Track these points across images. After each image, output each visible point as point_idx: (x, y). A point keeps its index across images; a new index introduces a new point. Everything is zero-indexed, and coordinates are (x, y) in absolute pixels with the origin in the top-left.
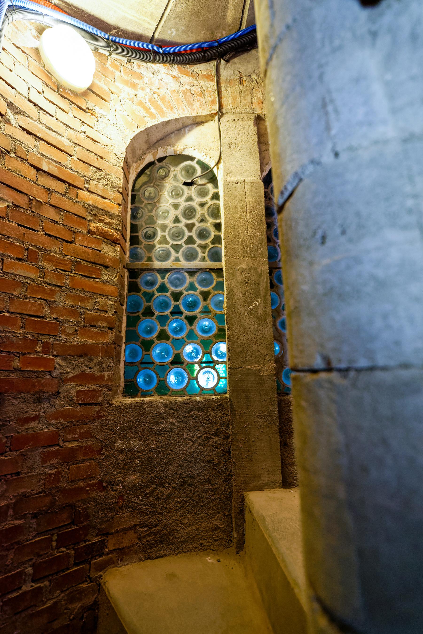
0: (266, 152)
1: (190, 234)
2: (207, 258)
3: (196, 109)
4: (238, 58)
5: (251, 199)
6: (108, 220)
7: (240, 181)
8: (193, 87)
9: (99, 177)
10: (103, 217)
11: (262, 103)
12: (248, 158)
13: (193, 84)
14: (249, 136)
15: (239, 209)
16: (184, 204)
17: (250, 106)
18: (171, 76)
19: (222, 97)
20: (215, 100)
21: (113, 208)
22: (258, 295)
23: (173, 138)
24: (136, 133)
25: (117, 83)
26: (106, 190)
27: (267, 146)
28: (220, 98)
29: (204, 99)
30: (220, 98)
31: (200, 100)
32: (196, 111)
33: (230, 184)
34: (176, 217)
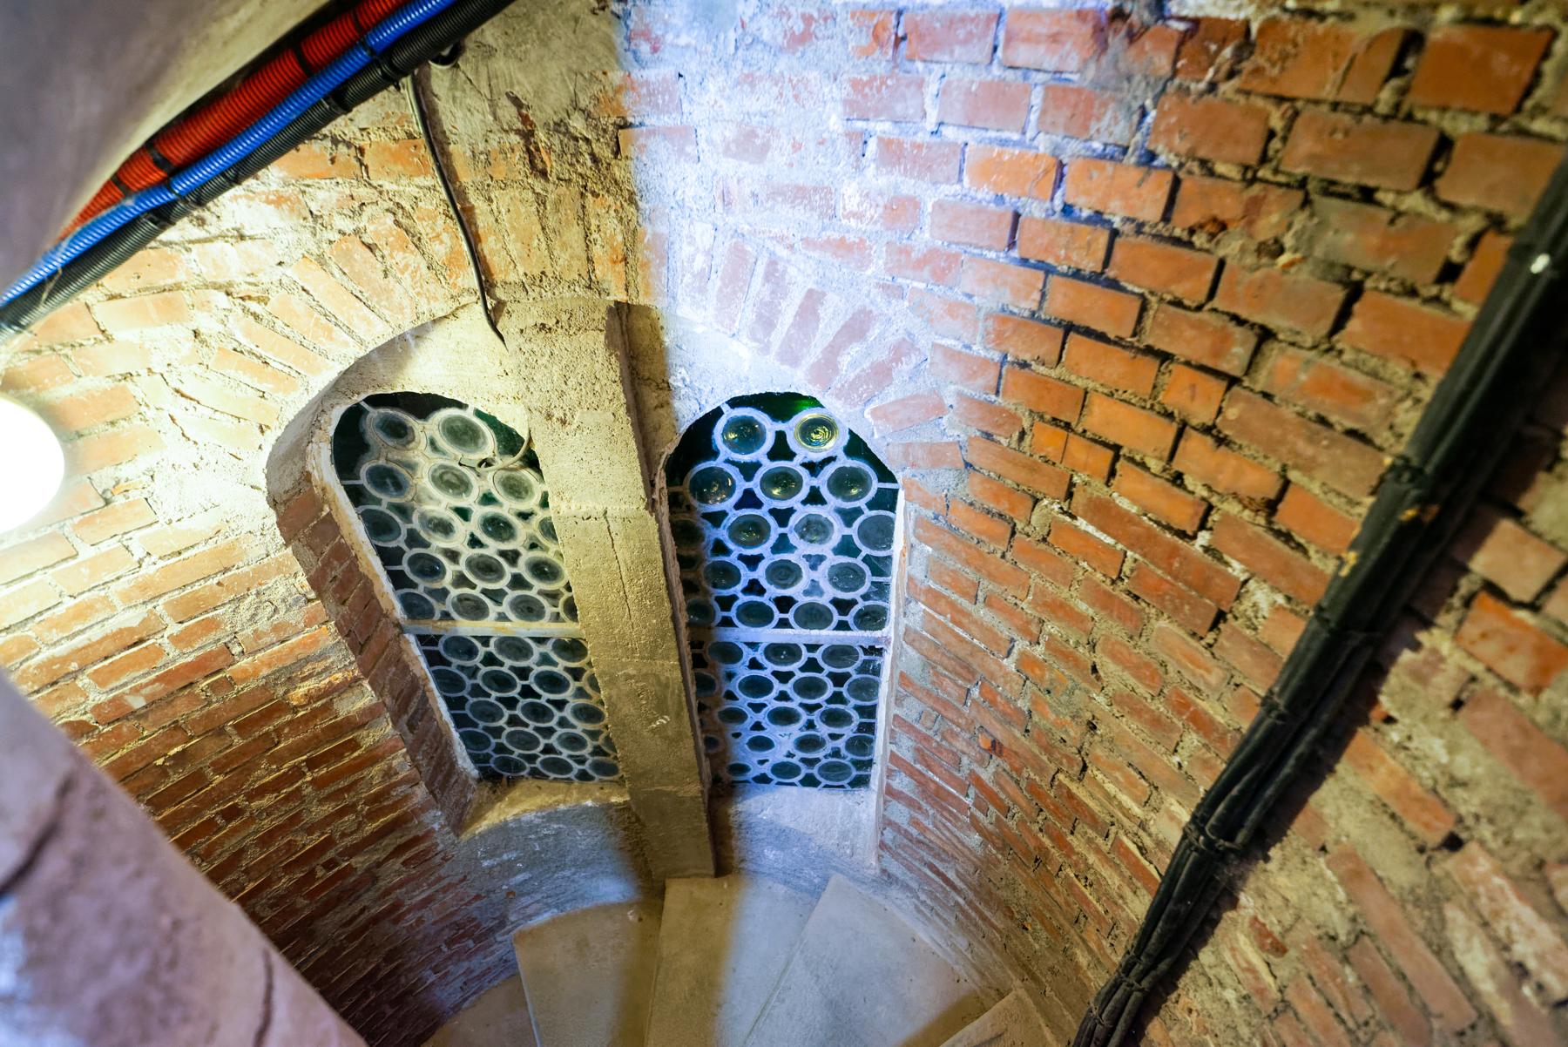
0: (660, 411)
1: (515, 571)
2: (563, 615)
3: (406, 302)
4: (496, 19)
5: (627, 555)
6: (319, 667)
7: (594, 515)
8: (365, 217)
9: (248, 615)
10: (307, 670)
11: (625, 259)
12: (605, 454)
13: (356, 205)
14: (597, 387)
15: (604, 575)
16: (479, 512)
17: (584, 274)
18: (269, 202)
19: (481, 231)
20: (460, 253)
21: (316, 642)
22: (662, 713)
23: (380, 365)
24: (268, 449)
25: (118, 335)
26: (279, 622)
27: (663, 394)
28: (473, 240)
29: (419, 256)
30: (473, 240)
31: (407, 266)
32: (408, 311)
33: (572, 521)
34: (472, 535)
